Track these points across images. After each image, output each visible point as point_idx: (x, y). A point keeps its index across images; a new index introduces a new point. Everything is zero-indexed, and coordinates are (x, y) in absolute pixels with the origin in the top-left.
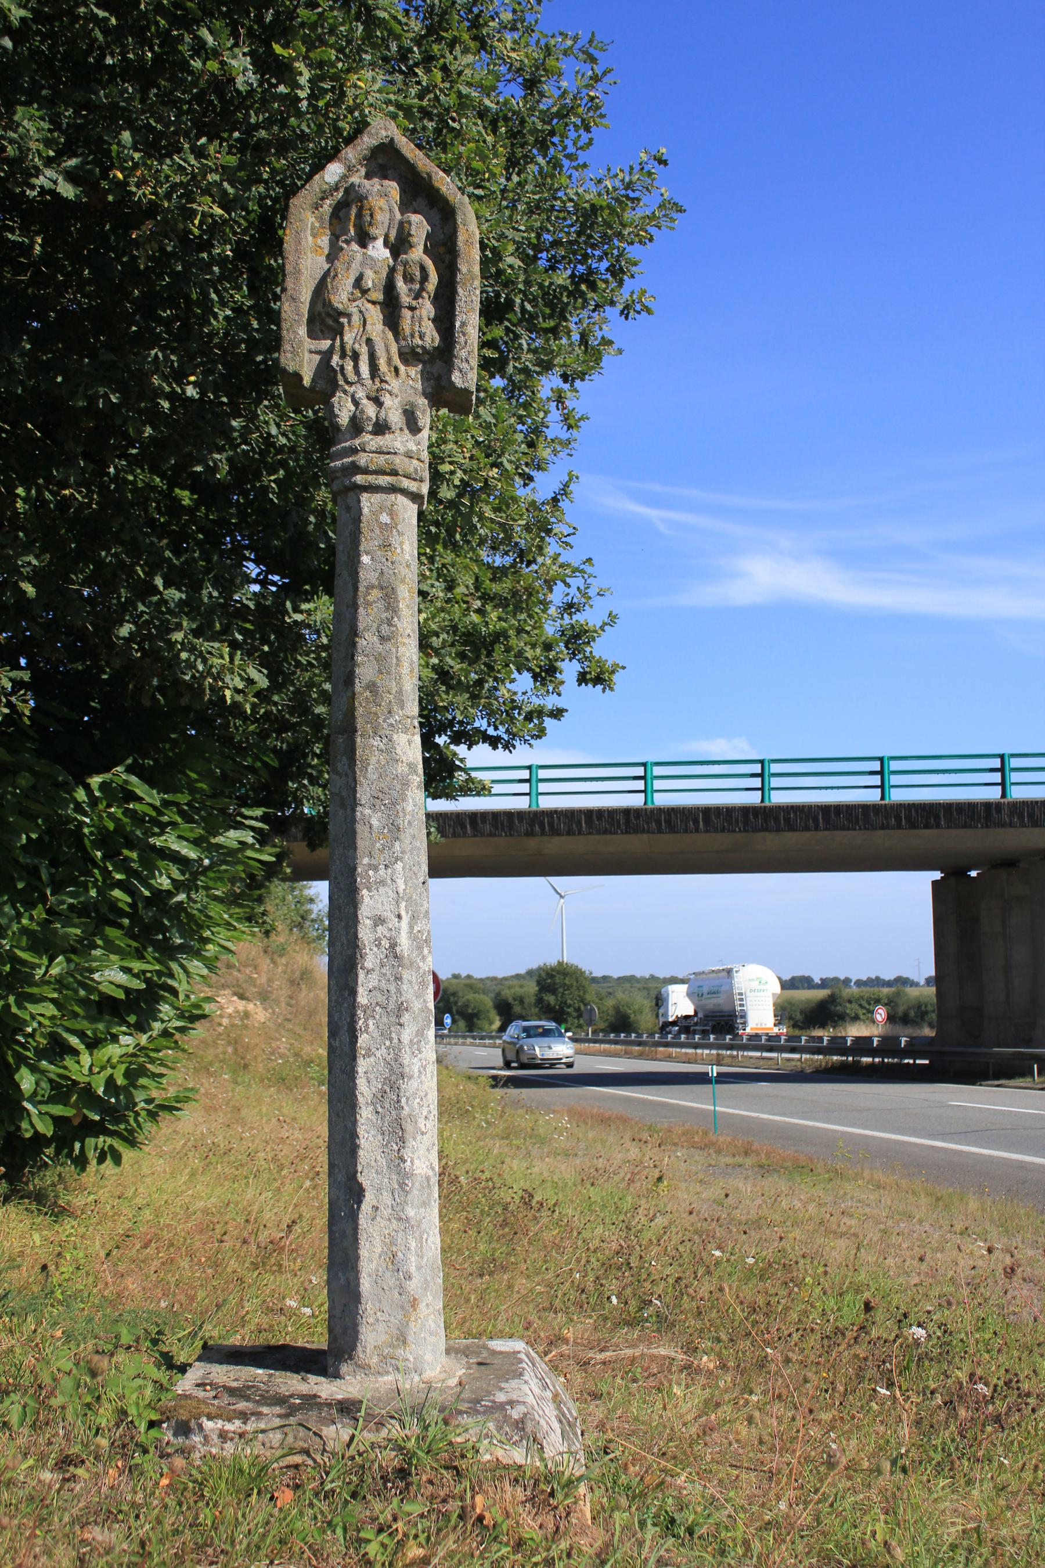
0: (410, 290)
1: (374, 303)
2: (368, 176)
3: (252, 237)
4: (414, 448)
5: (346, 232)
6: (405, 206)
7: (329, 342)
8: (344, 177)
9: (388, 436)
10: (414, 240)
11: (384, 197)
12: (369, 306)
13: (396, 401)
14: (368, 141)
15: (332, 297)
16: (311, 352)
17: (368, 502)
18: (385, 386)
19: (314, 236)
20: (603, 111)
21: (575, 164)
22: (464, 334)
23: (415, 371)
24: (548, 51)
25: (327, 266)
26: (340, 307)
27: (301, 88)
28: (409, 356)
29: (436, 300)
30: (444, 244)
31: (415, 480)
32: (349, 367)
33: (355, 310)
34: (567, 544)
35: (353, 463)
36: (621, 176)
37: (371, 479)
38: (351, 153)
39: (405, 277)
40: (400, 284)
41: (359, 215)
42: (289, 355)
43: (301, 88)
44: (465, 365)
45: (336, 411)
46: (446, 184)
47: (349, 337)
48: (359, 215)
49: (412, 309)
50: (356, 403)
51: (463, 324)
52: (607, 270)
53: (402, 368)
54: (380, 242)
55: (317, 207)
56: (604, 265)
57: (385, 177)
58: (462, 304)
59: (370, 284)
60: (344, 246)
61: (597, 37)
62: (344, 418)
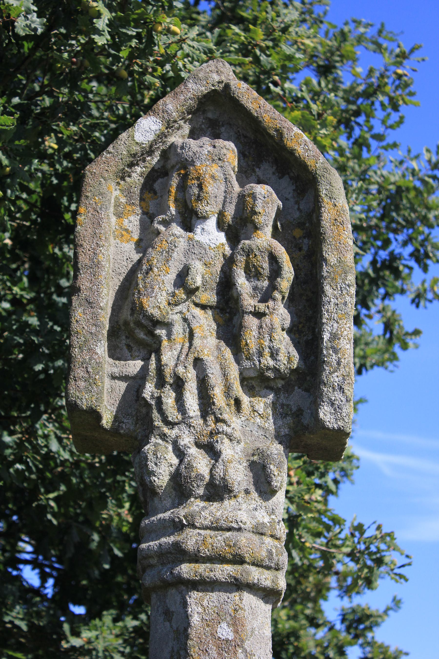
0: (255, 289)
1: (203, 307)
2: (193, 135)
3: (34, 222)
4: (266, 520)
5: (164, 210)
6: (246, 173)
7: (139, 363)
8: (162, 136)
9: (228, 504)
10: (260, 219)
11: (217, 163)
12: (197, 311)
13: (239, 448)
14: (193, 89)
15: (144, 300)
16: (113, 377)
17: (199, 606)
18: (222, 427)
19: (119, 215)
20: (412, 88)
21: (384, 144)
22: (336, 351)
23: (263, 404)
24: (343, 36)
25: (136, 257)
26: (156, 313)
27: (99, 33)
28: (256, 382)
29: (291, 302)
30: (301, 225)
31: (268, 568)
32: (169, 400)
33: (177, 318)
34: (401, 576)
35: (177, 545)
36: (426, 156)
37: (202, 569)
38: (171, 105)
39: (247, 270)
40: (242, 281)
41: (183, 187)
42: (82, 384)
43: (99, 33)
44: (337, 396)
45: (151, 466)
46: (300, 142)
47: (168, 357)
48: (183, 187)
49: (259, 315)
50: (180, 453)
51: (334, 337)
52: (411, 255)
53: (245, 399)
54: (212, 223)
55: (123, 176)
56: (410, 249)
57: (216, 136)
58: (331, 307)
59: (199, 282)
60: (162, 228)
61: (388, 28)
62: (162, 476)
